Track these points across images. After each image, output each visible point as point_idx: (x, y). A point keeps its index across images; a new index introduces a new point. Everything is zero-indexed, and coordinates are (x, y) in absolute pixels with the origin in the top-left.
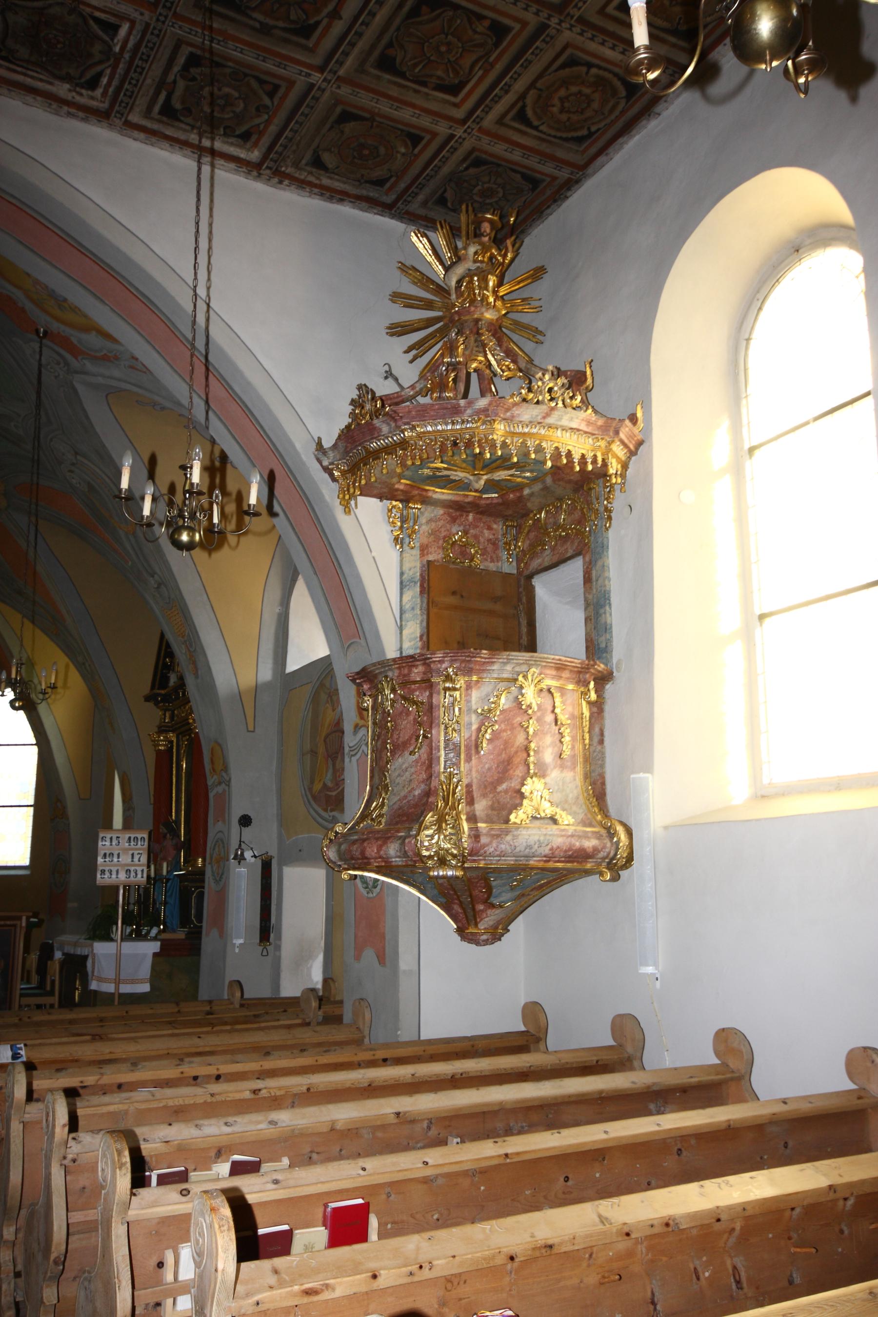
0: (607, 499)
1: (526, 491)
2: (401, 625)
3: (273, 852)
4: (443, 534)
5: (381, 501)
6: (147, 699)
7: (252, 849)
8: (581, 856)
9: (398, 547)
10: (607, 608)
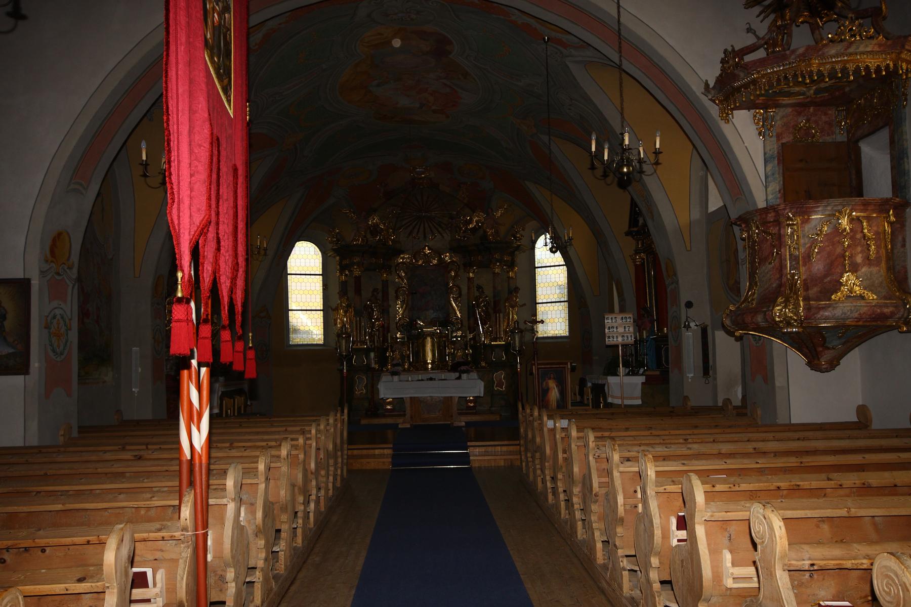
0: (903, 87)
1: (847, 89)
2: (766, 185)
3: (708, 322)
4: (792, 124)
5: (749, 111)
6: (627, 234)
7: (694, 321)
8: (883, 317)
9: (761, 137)
10: (906, 160)
